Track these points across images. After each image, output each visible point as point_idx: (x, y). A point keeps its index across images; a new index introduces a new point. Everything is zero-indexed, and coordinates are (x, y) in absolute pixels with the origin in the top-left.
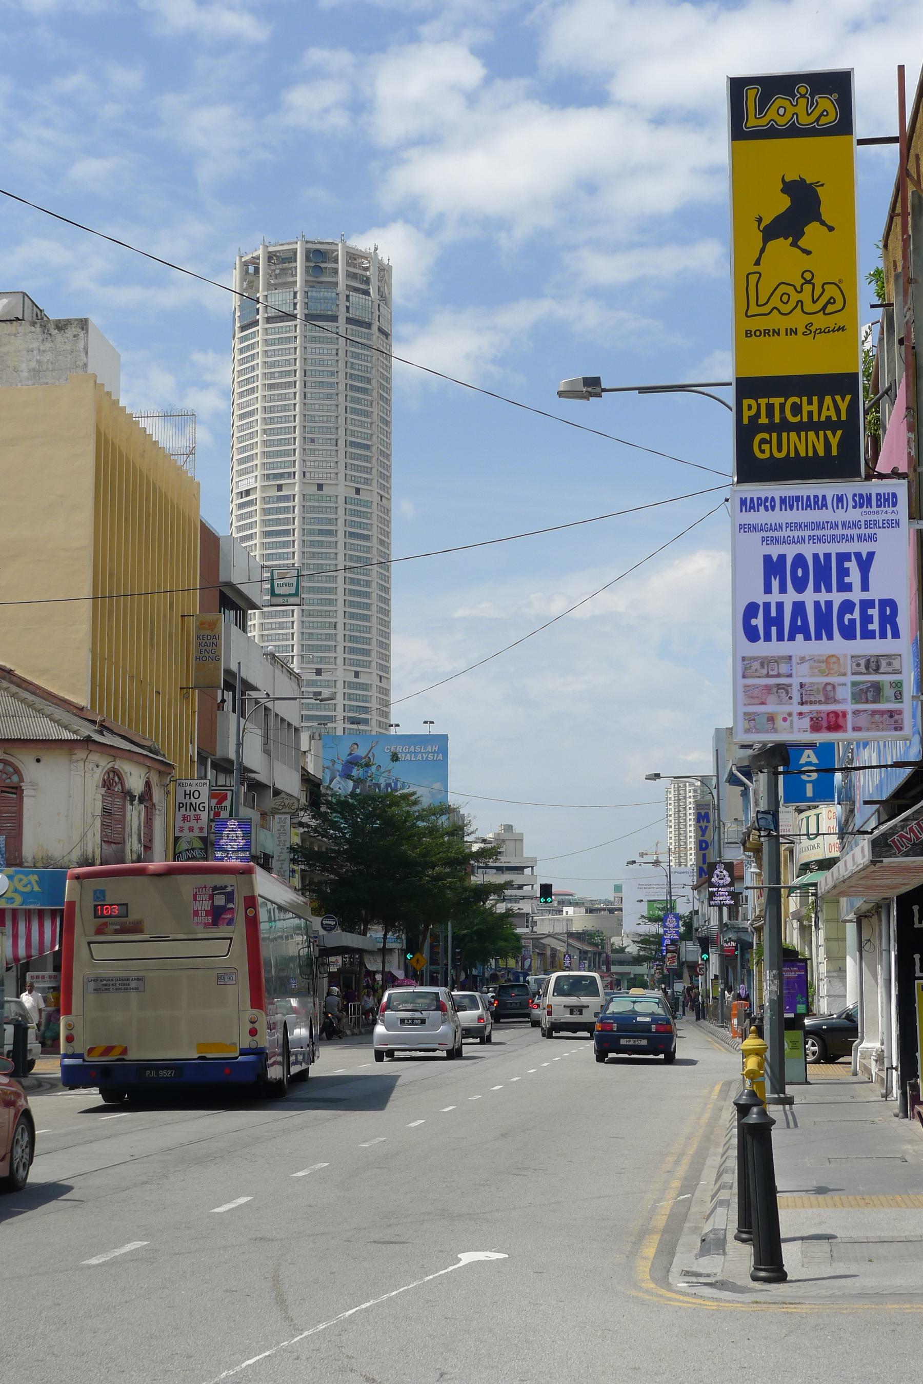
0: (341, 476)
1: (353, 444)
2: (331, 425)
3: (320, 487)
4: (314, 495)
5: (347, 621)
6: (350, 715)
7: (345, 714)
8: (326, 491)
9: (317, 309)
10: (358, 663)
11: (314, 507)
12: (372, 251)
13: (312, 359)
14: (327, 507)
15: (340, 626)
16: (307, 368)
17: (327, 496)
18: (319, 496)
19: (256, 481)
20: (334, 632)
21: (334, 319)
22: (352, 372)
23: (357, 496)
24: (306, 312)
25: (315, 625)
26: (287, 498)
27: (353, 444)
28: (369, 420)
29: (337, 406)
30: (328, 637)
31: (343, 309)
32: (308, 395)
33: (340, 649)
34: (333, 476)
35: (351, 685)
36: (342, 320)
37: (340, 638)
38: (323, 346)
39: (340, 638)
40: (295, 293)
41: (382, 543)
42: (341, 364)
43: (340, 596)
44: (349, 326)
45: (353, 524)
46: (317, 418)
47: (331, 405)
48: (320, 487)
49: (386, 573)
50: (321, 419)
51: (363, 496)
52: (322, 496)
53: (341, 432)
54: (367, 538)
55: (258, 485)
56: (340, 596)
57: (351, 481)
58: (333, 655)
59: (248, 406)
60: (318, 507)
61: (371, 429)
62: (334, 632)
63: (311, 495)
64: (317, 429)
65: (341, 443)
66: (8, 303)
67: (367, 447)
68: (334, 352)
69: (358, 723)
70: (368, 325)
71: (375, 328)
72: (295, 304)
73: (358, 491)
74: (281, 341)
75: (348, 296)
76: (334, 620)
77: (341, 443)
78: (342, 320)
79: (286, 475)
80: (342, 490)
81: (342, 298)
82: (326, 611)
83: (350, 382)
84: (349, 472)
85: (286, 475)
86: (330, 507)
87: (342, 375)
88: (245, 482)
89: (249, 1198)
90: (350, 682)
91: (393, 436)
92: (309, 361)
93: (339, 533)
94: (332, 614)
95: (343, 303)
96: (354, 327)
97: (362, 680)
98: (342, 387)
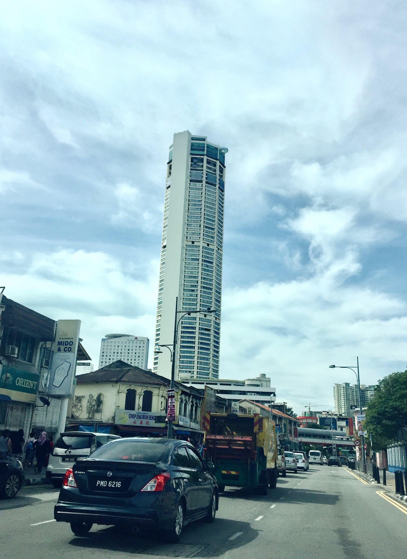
0: (201, 239)
1: (206, 227)
3: (193, 242)
5: (199, 356)
8: (196, 244)
20: (196, 298)
21: (201, 181)
27: (206, 227)
30: (194, 300)
31: (204, 186)
32: (190, 209)
34: (197, 264)
39: (199, 300)
41: (218, 270)
42: (203, 198)
43: (196, 345)
44: (207, 185)
45: (206, 257)
48: (193, 242)
49: (217, 359)
51: (211, 247)
54: (211, 289)
56: (196, 345)
58: (193, 365)
62: (196, 298)
65: (202, 226)
66: (77, 440)
68: (200, 193)
73: (208, 245)
77: (202, 226)
80: (202, 244)
84: (204, 237)
87: (203, 202)
89: (112, 526)
93: (195, 352)
97: (211, 247)
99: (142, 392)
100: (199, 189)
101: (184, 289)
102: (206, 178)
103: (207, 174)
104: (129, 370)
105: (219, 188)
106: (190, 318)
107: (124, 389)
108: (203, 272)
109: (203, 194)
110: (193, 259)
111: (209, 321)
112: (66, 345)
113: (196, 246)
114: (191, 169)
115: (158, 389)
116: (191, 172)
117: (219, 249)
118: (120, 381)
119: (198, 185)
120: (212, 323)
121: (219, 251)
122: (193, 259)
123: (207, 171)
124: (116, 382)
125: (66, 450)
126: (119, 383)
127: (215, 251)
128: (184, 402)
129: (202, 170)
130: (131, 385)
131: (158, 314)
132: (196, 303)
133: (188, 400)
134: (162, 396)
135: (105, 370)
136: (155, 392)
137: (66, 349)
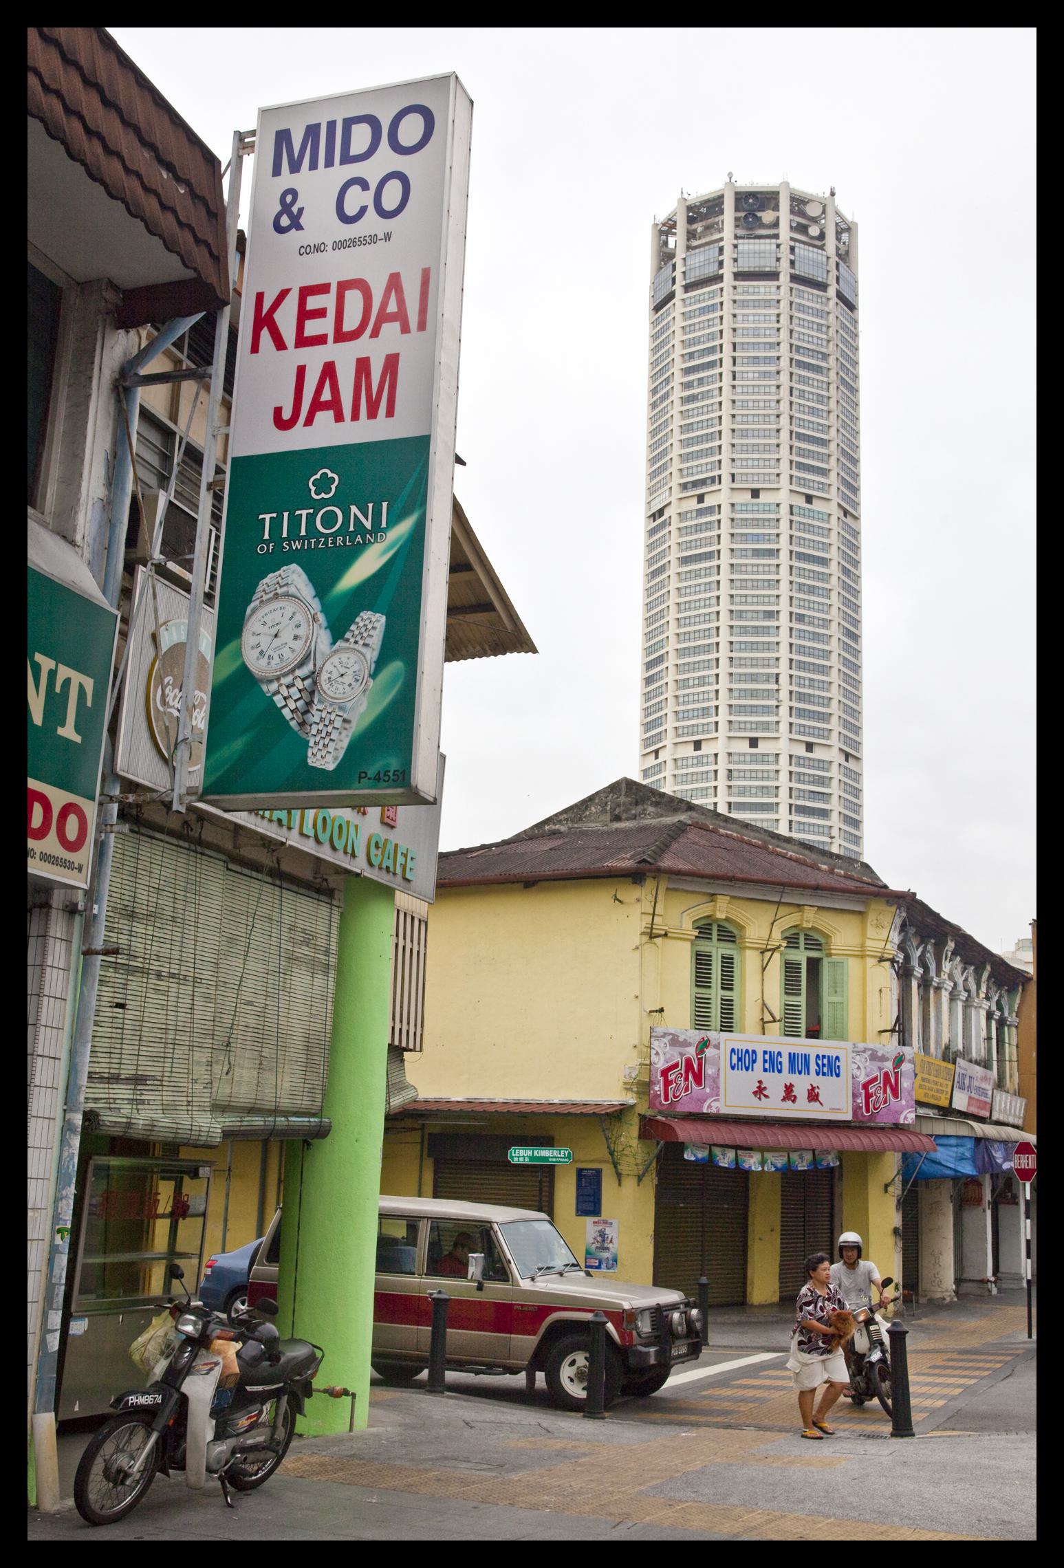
2: (771, 412)
4: (744, 755)
6: (800, 802)
7: (792, 801)
9: (746, 265)
10: (812, 731)
11: (746, 519)
12: (828, 194)
13: (743, 329)
14: (764, 520)
15: (784, 679)
16: (737, 340)
17: (764, 504)
18: (753, 504)
19: (670, 495)
21: (774, 276)
22: (800, 344)
23: (808, 506)
24: (736, 270)
25: (748, 726)
26: (710, 510)
28: (825, 408)
29: (778, 387)
33: (784, 710)
34: (773, 463)
35: (800, 761)
36: (784, 278)
37: (784, 695)
38: (759, 311)
39: (784, 695)
40: (721, 250)
42: (784, 334)
44: (795, 286)
45: (802, 697)
46: (751, 404)
47: (770, 386)
50: (756, 463)
52: (758, 504)
53: (784, 420)
55: (673, 499)
57: (799, 733)
59: (656, 651)
60: (753, 519)
61: (827, 419)
63: (742, 504)
64: (751, 404)
67: (824, 443)
68: (774, 318)
69: (809, 710)
70: (822, 286)
71: (832, 292)
72: (721, 264)
74: (703, 311)
75: (792, 249)
76: (775, 671)
78: (784, 278)
79: (709, 481)
81: (785, 249)
82: (763, 659)
83: (797, 357)
85: (709, 481)
86: (769, 520)
88: (657, 500)
90: (799, 757)
91: (863, 518)
92: (739, 332)
94: (772, 647)
95: (785, 255)
96: (802, 288)
98: (784, 363)
99: (777, 935)
100: (767, 303)
101: (731, 659)
102: (792, 263)
103: (792, 249)
104: (681, 829)
105: (840, 295)
106: (756, 759)
107: (681, 914)
108: (795, 595)
109: (784, 319)
110: (757, 553)
111: (825, 765)
112: (347, 159)
113: (763, 758)
114: (736, 237)
115: (854, 921)
116: (736, 246)
117: (846, 513)
118: (658, 873)
119: (763, 289)
120: (834, 772)
121: (849, 520)
122: (757, 553)
123: (792, 239)
124: (636, 876)
125: (34, 126)
126: (650, 884)
127: (834, 520)
128: (964, 995)
129: (776, 236)
130: (712, 897)
131: (646, 746)
132: (775, 703)
133: (973, 987)
134: (881, 960)
135: (555, 834)
136: (843, 935)
137: (356, 199)
